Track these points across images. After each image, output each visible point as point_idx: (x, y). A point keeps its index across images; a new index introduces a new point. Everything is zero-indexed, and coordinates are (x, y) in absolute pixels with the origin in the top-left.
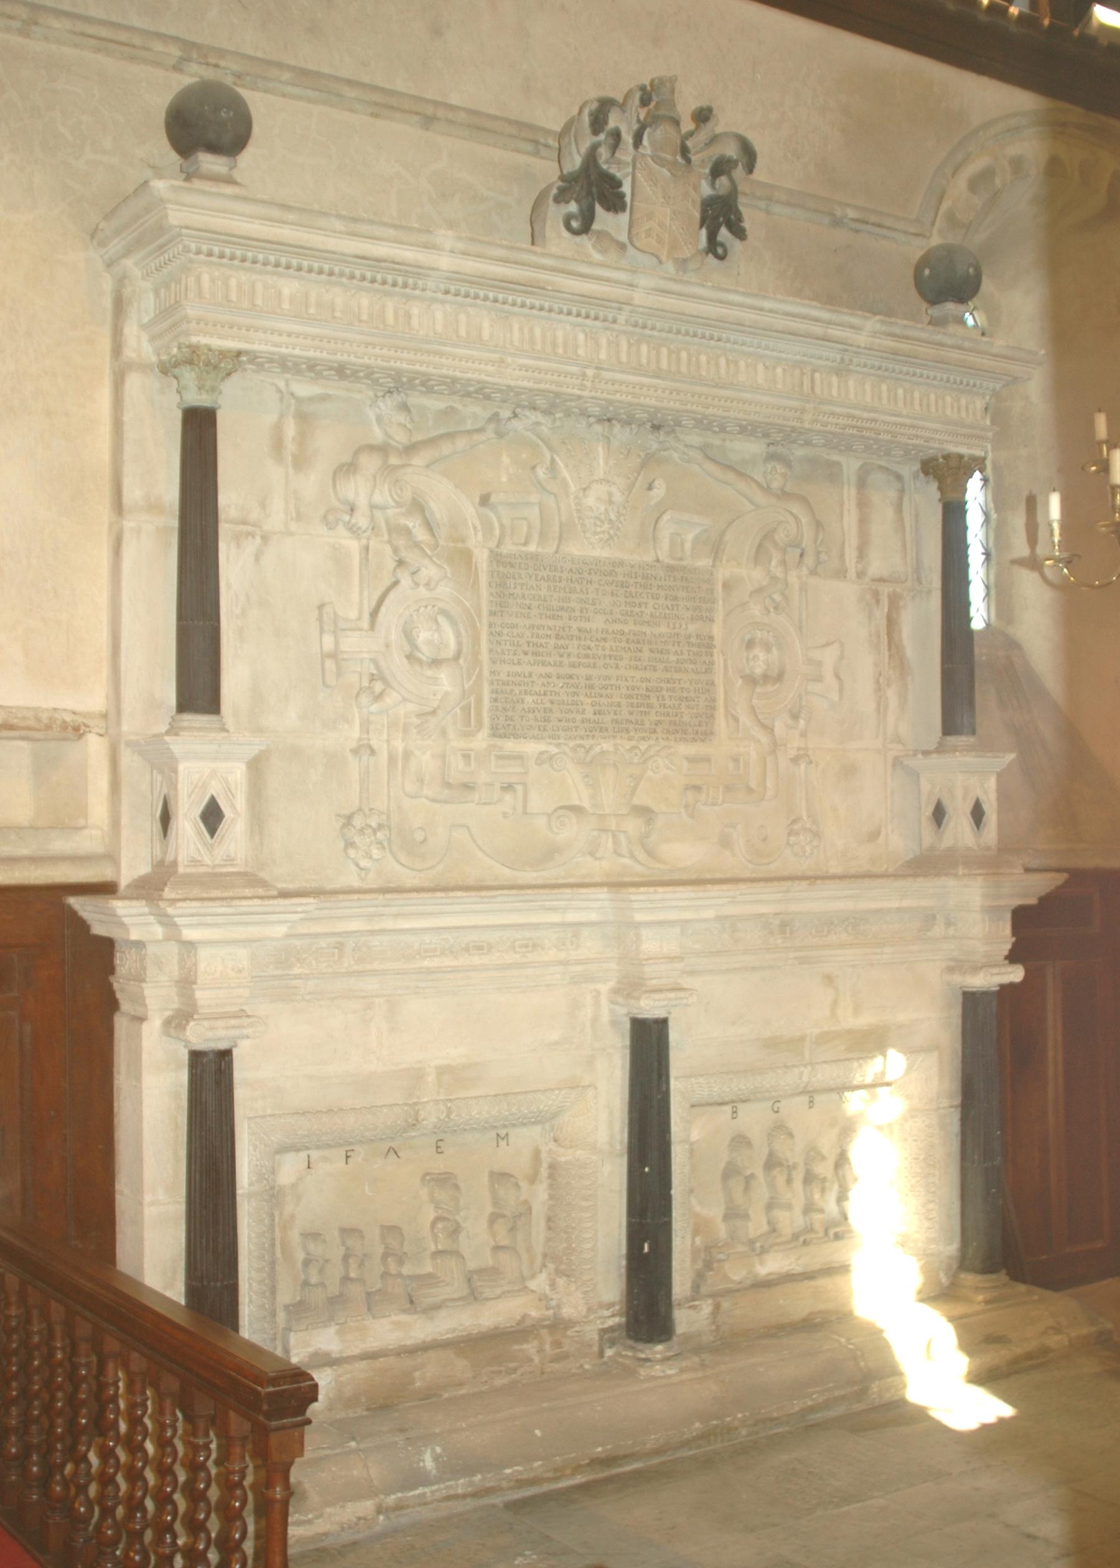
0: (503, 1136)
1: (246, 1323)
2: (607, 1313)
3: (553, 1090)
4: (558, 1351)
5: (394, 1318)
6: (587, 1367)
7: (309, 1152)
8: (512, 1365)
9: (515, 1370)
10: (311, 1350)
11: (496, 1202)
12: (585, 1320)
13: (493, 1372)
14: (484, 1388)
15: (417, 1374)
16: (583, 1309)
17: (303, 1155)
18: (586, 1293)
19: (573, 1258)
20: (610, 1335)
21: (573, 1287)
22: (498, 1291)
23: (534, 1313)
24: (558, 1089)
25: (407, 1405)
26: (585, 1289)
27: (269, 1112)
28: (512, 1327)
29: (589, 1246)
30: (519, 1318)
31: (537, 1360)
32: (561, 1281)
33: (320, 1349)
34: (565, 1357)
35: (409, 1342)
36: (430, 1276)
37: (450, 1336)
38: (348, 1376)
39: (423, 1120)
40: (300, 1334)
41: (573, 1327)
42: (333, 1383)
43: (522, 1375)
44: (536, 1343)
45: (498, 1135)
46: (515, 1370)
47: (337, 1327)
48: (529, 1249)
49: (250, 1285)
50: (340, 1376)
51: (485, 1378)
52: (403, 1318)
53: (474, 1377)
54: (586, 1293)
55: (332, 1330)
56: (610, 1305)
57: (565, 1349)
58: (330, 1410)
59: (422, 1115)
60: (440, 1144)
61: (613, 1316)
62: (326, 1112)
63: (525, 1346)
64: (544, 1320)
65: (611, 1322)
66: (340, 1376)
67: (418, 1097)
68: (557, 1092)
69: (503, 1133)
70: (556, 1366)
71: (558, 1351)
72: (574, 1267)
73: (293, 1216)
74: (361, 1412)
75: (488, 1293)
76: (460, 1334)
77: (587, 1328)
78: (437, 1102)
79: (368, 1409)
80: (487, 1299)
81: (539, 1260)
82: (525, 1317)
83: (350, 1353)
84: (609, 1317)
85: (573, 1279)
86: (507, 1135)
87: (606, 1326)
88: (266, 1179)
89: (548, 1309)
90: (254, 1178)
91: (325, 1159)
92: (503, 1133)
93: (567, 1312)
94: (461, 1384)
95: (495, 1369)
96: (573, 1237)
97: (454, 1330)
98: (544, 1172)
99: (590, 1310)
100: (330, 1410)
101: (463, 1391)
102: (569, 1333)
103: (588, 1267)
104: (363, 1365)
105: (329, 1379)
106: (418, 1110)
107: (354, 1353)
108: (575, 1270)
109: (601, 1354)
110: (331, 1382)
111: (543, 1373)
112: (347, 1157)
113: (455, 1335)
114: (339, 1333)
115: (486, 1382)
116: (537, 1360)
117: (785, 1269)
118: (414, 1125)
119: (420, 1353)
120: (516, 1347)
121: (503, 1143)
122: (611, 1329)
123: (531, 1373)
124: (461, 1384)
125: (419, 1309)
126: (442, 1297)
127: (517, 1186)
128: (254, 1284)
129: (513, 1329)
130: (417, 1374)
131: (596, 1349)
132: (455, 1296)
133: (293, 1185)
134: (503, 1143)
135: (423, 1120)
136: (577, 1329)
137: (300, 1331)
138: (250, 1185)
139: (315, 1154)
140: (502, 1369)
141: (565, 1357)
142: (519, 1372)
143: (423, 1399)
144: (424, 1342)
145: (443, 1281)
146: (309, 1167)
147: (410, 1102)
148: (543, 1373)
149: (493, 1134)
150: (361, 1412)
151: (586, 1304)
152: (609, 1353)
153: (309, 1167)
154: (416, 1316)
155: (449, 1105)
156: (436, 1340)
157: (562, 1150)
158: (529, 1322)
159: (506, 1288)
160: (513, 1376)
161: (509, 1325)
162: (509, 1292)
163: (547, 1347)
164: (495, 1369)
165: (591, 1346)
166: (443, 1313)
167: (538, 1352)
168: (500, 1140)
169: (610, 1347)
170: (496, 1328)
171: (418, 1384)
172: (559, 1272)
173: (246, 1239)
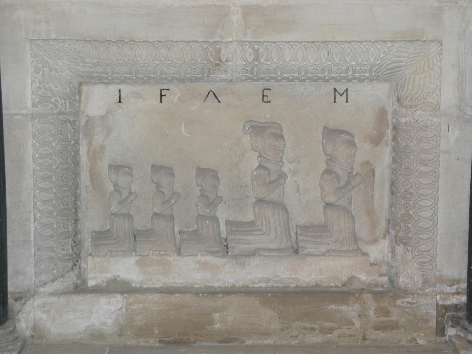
0: (341, 91)
1: (341, 308)
2: (448, 289)
3: (385, 42)
4: (385, 319)
5: (199, 258)
6: (420, 342)
7: (121, 87)
8: (328, 324)
9: (331, 330)
10: (109, 276)
11: (331, 159)
12: (420, 292)
13: (305, 328)
14: (294, 342)
15: (217, 316)
16: (418, 280)
17: (113, 88)
18: (421, 264)
19: (409, 225)
20: (453, 313)
21: (409, 256)
22: (323, 249)
23: (363, 277)
24: (392, 42)
25: (204, 344)
26: (420, 260)
27: (53, 36)
28: (336, 286)
29: (428, 214)
30: (345, 279)
31: (358, 324)
32: (400, 249)
33: (119, 276)
34: (394, 326)
35: (216, 285)
36: (252, 224)
37: (264, 285)
38: (140, 306)
39: (227, 61)
40: (98, 260)
41: (403, 297)
42: (124, 310)
43: (339, 337)
44: (357, 306)
45: (335, 90)
46: (331, 330)
47: (138, 258)
48: (370, 212)
49: (35, 203)
50: (131, 304)
51: (295, 333)
52: (211, 259)
53: (282, 330)
54: (421, 264)
55: (132, 260)
56: (452, 282)
57: (393, 318)
58: (120, 335)
59: (224, 54)
60: (266, 92)
61: (458, 293)
62: (115, 42)
63: (344, 308)
64: (377, 285)
65: (454, 300)
66: (131, 304)
67: (221, 37)
68: (390, 44)
69: (341, 88)
70: (382, 335)
71: (385, 319)
72: (410, 235)
73: (102, 148)
74: (152, 342)
75: (310, 249)
76: (275, 285)
77: (422, 301)
78: (241, 43)
79: (160, 341)
80: (308, 255)
81: (383, 225)
82: (352, 279)
83: (151, 286)
84: (453, 294)
85: (409, 248)
86: (347, 90)
87: (448, 303)
88: (52, 103)
89: (381, 275)
90: (37, 100)
91: (138, 95)
92: (341, 88)
93: (402, 281)
94: (266, 334)
95: (307, 325)
96: (411, 203)
97: (268, 280)
98: (389, 132)
99: (425, 282)
100: (120, 335)
101: (269, 342)
102: (399, 302)
103: (424, 236)
104: (157, 297)
105: (119, 306)
106: (220, 49)
107: (155, 286)
108: (410, 238)
109: (441, 331)
110: (121, 309)
111: (365, 339)
112: (161, 96)
113: (270, 284)
114: (138, 263)
115: (297, 336)
116: (358, 324)
117: (388, 188)
118: (218, 65)
119: (220, 295)
120: (333, 307)
121: (341, 100)
122: (456, 307)
123: (350, 336)
124: (266, 334)
125: (230, 254)
126: (257, 246)
127: (352, 144)
128: (38, 203)
129: (338, 289)
130: (217, 316)
131: (433, 324)
132: (273, 246)
133: (103, 117)
134: (341, 100)
135: (227, 61)
136: (410, 300)
137: (99, 256)
138: (34, 105)
139: (126, 89)
140: (316, 327)
141: (394, 326)
142: (336, 333)
143: (222, 342)
144: (233, 287)
145: (260, 230)
146: (120, 102)
147: (211, 41)
148: (365, 339)
149: (329, 88)
150: (152, 342)
151: (423, 275)
152: (451, 332)
153: (120, 102)
154: (225, 260)
155: (256, 47)
156: (248, 287)
157: (403, 111)
158: (356, 286)
159: (331, 247)
160: (329, 335)
161: (332, 284)
162: (334, 251)
163: (371, 313)
164: (307, 325)
165: (426, 321)
166: (256, 261)
167: (359, 316)
168: (338, 96)
169: (452, 327)
170: (317, 285)
171: (217, 326)
172: (397, 240)
173: (31, 160)
